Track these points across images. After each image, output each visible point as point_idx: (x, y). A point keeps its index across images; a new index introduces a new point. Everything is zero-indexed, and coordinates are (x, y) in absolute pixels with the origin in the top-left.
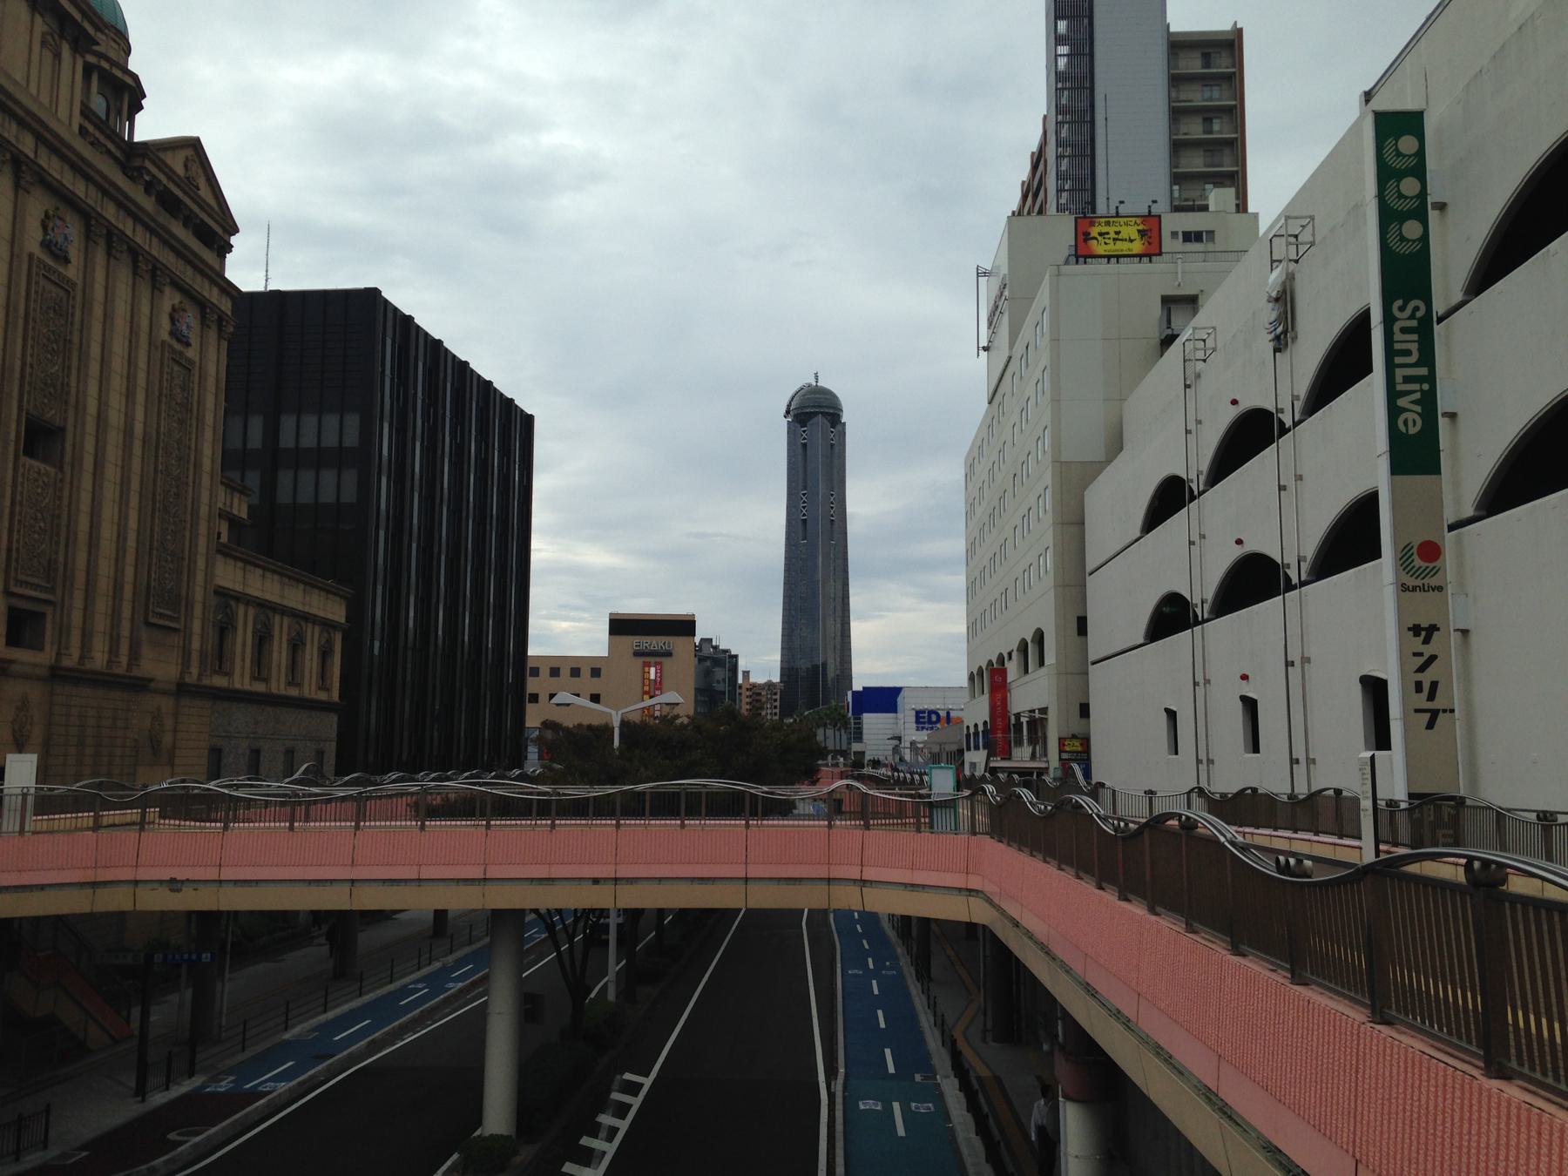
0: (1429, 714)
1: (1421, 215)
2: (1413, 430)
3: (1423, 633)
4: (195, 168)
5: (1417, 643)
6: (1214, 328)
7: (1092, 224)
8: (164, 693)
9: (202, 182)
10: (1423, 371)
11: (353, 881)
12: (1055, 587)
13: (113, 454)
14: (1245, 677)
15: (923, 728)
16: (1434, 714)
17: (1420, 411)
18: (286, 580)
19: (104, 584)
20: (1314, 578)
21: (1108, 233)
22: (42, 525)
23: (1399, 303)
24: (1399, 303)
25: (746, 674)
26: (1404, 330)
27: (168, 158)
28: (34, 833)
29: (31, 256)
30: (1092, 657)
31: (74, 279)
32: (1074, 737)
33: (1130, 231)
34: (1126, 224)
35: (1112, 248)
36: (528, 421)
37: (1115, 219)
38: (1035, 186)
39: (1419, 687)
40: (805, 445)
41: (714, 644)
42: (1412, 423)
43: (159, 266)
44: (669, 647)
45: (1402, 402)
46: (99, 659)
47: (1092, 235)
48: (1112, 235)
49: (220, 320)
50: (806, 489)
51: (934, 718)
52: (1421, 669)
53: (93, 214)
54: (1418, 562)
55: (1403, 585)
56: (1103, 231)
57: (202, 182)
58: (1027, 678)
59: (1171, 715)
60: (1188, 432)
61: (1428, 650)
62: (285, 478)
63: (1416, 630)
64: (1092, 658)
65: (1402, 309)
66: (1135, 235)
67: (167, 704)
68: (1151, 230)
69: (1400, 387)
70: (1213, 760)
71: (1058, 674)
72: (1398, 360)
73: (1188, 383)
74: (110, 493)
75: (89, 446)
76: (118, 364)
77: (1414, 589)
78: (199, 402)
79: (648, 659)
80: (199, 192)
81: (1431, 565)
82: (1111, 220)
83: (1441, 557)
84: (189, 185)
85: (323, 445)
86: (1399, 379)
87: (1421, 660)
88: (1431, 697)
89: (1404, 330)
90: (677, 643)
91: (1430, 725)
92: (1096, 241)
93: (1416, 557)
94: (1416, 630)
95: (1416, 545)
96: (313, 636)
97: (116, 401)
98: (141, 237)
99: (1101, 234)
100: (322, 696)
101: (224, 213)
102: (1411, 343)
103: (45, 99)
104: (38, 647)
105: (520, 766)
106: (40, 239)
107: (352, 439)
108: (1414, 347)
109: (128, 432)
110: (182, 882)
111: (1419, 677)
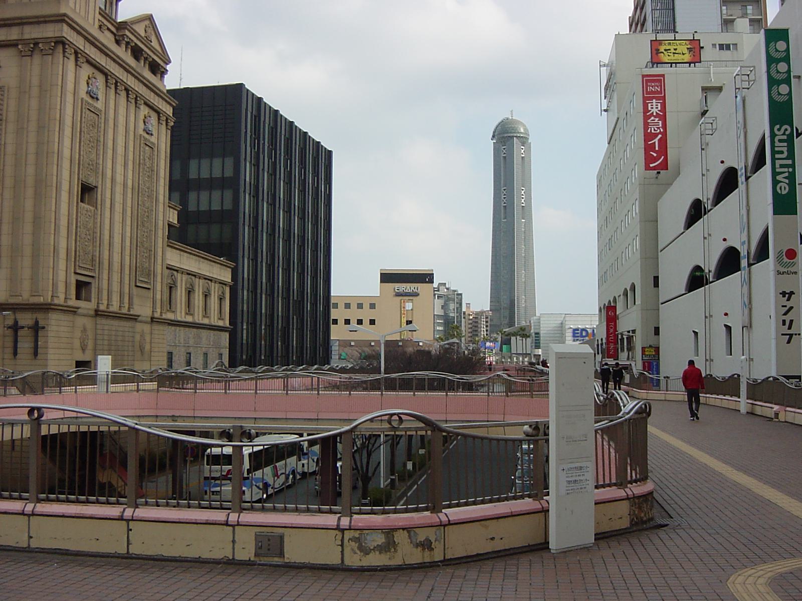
0: (788, 336)
1: (788, 81)
2: (784, 192)
3: (787, 295)
4: (150, 30)
6: (716, 118)
7: (660, 44)
8: (146, 322)
9: (153, 38)
10: (790, 162)
11: (255, 418)
12: (641, 258)
13: (118, 198)
14: (726, 314)
15: (577, 340)
16: (791, 335)
17: (787, 182)
19: (116, 266)
21: (670, 50)
22: (89, 237)
23: (778, 126)
24: (778, 126)
26: (780, 141)
27: (135, 27)
28: (112, 392)
29: (82, 99)
31: (100, 108)
32: (650, 346)
33: (683, 49)
34: (680, 44)
35: (672, 58)
37: (674, 42)
38: (641, 3)
39: (784, 322)
40: (505, 158)
41: (447, 286)
42: (784, 189)
43: (139, 95)
44: (417, 290)
45: (779, 178)
46: (115, 308)
47: (660, 51)
49: (167, 119)
50: (505, 186)
51: (584, 334)
52: (785, 314)
53: (109, 74)
54: (786, 260)
55: (778, 271)
56: (667, 48)
57: (153, 38)
58: (628, 311)
59: (696, 333)
60: (703, 175)
61: (789, 304)
62: (192, 196)
63: (784, 294)
64: (661, 301)
65: (779, 130)
66: (686, 51)
67: (147, 328)
68: (694, 48)
70: (752, 359)
71: (642, 310)
72: (777, 156)
73: (703, 147)
74: (118, 217)
75: (108, 195)
76: (120, 150)
77: (783, 273)
78: (157, 166)
80: (152, 44)
81: (792, 261)
82: (671, 42)
83: (796, 258)
84: (147, 41)
85: (201, 177)
86: (777, 166)
87: (786, 309)
88: (790, 328)
89: (780, 141)
90: (420, 287)
91: (789, 342)
92: (662, 54)
93: (784, 257)
94: (784, 294)
96: (215, 289)
97: (119, 169)
98: (131, 82)
99: (665, 50)
100: (221, 323)
101: (164, 53)
103: (83, 13)
104: (88, 299)
105: (328, 364)
106: (86, 90)
107: (229, 173)
109: (125, 185)
110: (177, 416)
111: (784, 317)
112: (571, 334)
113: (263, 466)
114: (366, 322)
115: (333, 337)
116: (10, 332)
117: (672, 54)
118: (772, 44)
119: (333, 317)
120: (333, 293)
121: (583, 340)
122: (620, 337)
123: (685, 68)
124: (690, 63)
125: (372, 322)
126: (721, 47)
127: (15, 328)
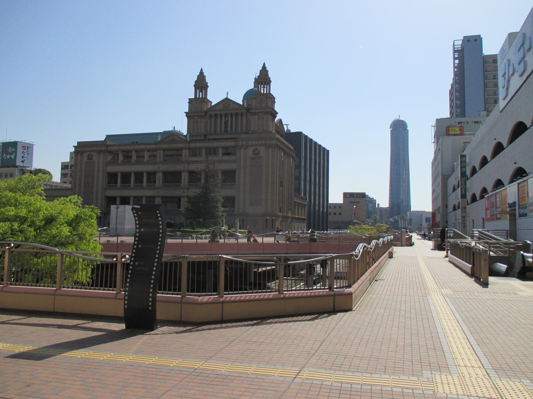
2: (463, 193)
5: (463, 218)
7: (450, 128)
10: (465, 186)
16: (464, 227)
25: (378, 205)
26: (463, 181)
30: (448, 212)
39: (463, 223)
42: (463, 192)
54: (463, 209)
61: (464, 219)
63: (463, 217)
66: (458, 130)
69: (462, 188)
88: (464, 224)
89: (463, 181)
94: (463, 217)
102: (464, 183)
108: (464, 183)
112: (425, 220)
113: (271, 281)
114: (338, 214)
115: (329, 220)
126: (475, 122)
127: (267, 220)
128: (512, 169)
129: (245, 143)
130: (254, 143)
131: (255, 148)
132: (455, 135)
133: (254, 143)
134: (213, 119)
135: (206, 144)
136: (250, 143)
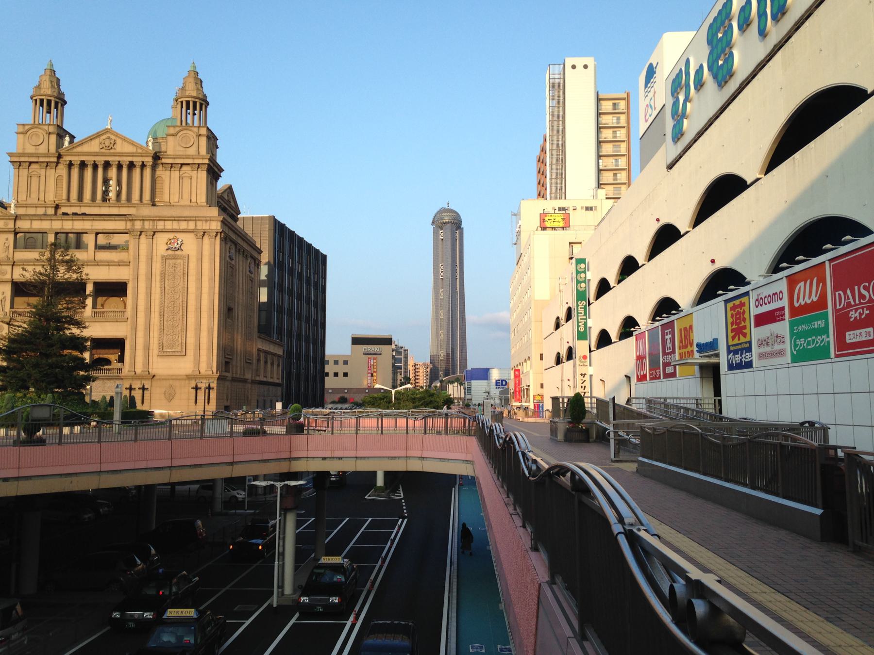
2: (582, 331)
4: (230, 195)
7: (546, 216)
9: (231, 200)
10: (585, 317)
15: (499, 388)
18: (264, 341)
20: (618, 340)
23: (580, 302)
24: (580, 302)
26: (581, 308)
36: (324, 257)
42: (582, 329)
45: (580, 324)
48: (553, 220)
51: (504, 383)
52: (582, 383)
54: (582, 360)
61: (584, 379)
65: (580, 303)
66: (561, 220)
67: (249, 386)
69: (580, 321)
72: (579, 315)
79: (370, 356)
86: (579, 319)
87: (582, 381)
88: (584, 389)
89: (581, 308)
90: (386, 349)
95: (582, 356)
99: (549, 220)
102: (582, 311)
108: (583, 312)
109: (242, 305)
111: (582, 385)
114: (341, 375)
115: (327, 386)
116: (194, 391)
117: (552, 222)
118: (579, 265)
119: (326, 371)
120: (327, 353)
121: (503, 388)
122: (522, 389)
123: (560, 232)
124: (563, 228)
125: (346, 375)
126: (587, 209)
128: (703, 272)
129: (148, 225)
130: (169, 225)
131: (171, 236)
132: (554, 228)
133: (169, 225)
134: (75, 172)
135: (57, 225)
136: (160, 225)
